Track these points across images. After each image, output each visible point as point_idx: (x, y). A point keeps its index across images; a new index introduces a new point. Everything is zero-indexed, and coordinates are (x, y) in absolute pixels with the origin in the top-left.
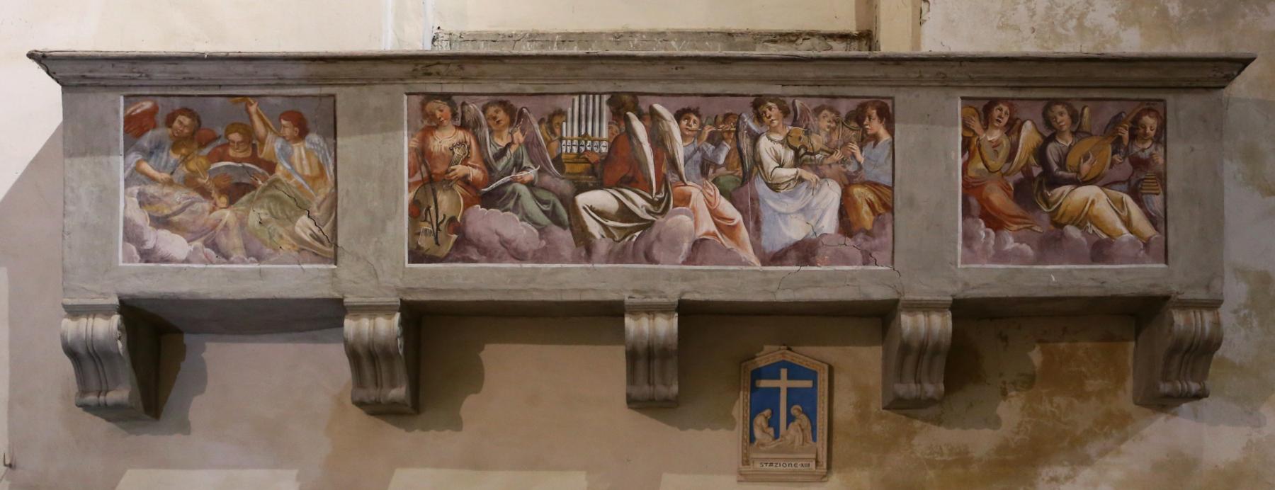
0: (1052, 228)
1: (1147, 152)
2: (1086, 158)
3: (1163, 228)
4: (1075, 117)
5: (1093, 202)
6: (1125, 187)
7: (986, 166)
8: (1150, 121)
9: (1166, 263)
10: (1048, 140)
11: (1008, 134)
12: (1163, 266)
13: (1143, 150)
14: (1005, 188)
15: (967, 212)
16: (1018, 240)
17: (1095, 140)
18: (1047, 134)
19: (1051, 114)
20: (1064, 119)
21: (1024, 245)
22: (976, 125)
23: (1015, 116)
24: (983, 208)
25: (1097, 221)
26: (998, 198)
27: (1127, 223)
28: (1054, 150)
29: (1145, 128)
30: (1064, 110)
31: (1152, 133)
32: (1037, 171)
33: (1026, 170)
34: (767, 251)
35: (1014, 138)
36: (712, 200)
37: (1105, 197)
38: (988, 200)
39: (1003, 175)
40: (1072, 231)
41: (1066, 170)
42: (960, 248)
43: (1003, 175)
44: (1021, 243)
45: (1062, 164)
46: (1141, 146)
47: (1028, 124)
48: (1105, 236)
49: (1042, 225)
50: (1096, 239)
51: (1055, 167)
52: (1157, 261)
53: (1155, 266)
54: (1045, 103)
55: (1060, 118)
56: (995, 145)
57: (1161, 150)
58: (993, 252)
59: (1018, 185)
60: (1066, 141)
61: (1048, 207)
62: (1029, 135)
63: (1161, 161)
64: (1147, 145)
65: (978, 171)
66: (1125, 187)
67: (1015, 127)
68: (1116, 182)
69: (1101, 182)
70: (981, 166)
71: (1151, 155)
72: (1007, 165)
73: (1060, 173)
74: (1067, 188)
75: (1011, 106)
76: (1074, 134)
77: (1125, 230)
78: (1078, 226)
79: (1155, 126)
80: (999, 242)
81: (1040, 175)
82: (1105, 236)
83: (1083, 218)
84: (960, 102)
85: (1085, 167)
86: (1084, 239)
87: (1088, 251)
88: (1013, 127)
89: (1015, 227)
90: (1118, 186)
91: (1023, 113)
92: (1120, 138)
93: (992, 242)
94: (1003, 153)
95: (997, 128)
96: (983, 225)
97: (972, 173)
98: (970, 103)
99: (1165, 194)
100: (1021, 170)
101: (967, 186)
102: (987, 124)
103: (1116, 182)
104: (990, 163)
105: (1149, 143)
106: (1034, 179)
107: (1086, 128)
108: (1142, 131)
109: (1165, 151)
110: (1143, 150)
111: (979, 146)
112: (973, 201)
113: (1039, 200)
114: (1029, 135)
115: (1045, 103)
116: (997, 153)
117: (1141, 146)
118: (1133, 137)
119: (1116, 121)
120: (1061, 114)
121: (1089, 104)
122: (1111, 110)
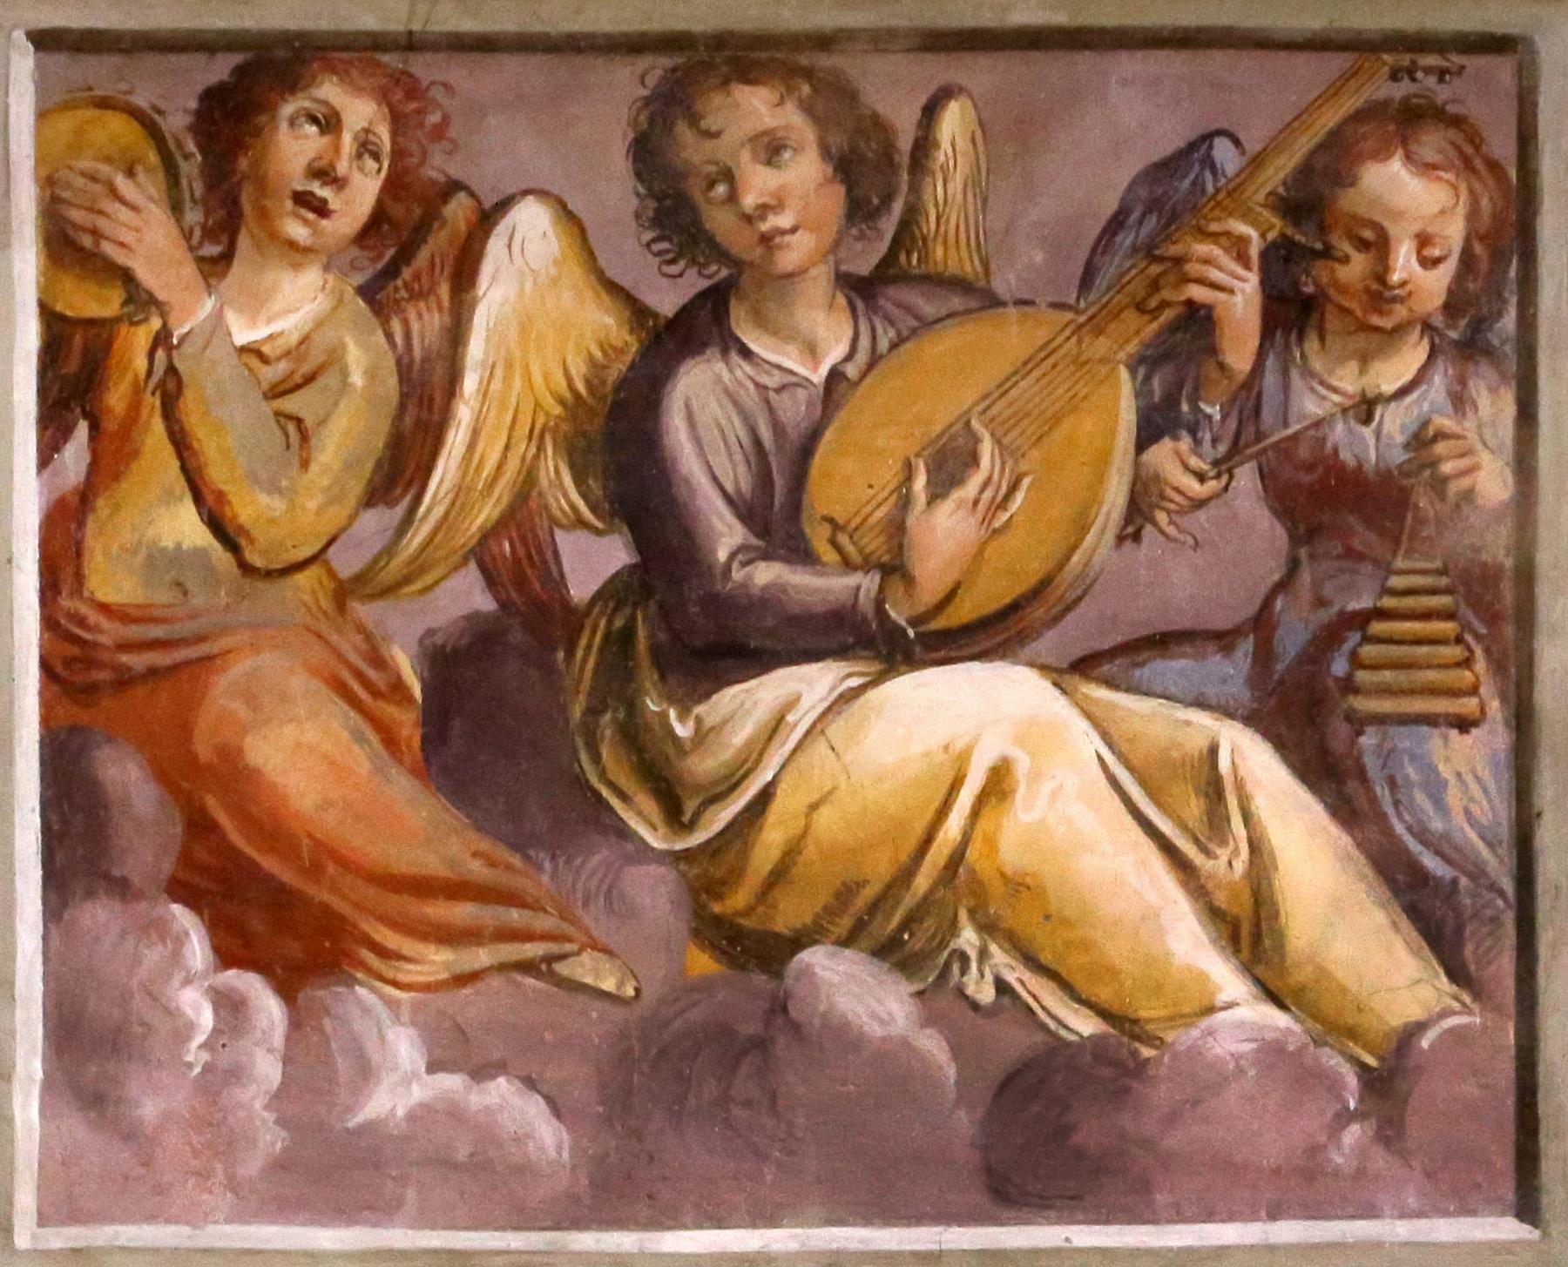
0: (702, 963)
1: (1395, 422)
2: (950, 463)
3: (1505, 965)
4: (871, 171)
5: (998, 784)
6: (1231, 671)
7: (217, 524)
8: (1413, 198)
9: (1528, 1208)
10: (673, 339)
11: (377, 295)
12: (1509, 1229)
13: (1366, 408)
14: (360, 686)
15: (78, 846)
16: (453, 1050)
17: (1012, 338)
18: (667, 300)
19: (690, 149)
20: (782, 183)
21: (501, 1095)
22: (149, 237)
23: (437, 165)
24: (199, 825)
25: (1022, 913)
26: (309, 754)
27: (1250, 930)
28: (712, 410)
29: (1380, 246)
30: (791, 119)
31: (1433, 285)
32: (592, 561)
33: (515, 557)
34: (248, 739)
35: (426, 323)
36: (456, 559)
37: (1089, 743)
38: (234, 775)
39: (344, 592)
40: (852, 990)
41: (801, 554)
42: (27, 1109)
43: (344, 592)
44: (481, 1073)
45: (776, 520)
46: (1348, 380)
47: (531, 224)
48: (1085, 1025)
49: (630, 949)
50: (1015, 1043)
51: (725, 535)
52: (1493, 1205)
53: (1446, 1230)
54: (657, 66)
55: (758, 183)
56: (292, 379)
57: (1494, 406)
58: (271, 1139)
59: (456, 664)
60: (808, 340)
61: (675, 816)
62: (534, 307)
63: (1493, 482)
64: (1394, 371)
65: (167, 564)
66: (1231, 671)
67: (437, 245)
68: (1162, 642)
69: (1046, 645)
70: (184, 527)
71: (1422, 440)
72: (376, 523)
73: (765, 574)
74: (812, 684)
75: (404, 101)
76: (861, 290)
77: (1227, 979)
78: (893, 953)
79: (1454, 232)
80: (317, 1069)
81: (615, 592)
82: (1085, 1025)
83: (917, 907)
84: (24, 63)
85: (944, 531)
86: (933, 1045)
87: (965, 1122)
88: (416, 246)
89: (438, 960)
90: (1173, 668)
91: (494, 136)
92: (1199, 323)
93: (268, 1070)
94: (349, 429)
95: (296, 253)
96: (198, 950)
97: (112, 579)
98: (99, 71)
99: (1523, 720)
100: (481, 554)
101: (73, 669)
102: (225, 221)
103: (1162, 642)
104: (251, 507)
105: (1409, 359)
106: (572, 620)
107: (950, 257)
108: (1356, 268)
109: (1527, 414)
110: (1366, 408)
111: (171, 389)
112: (125, 775)
113: (609, 769)
114: (534, 307)
115: (657, 66)
116: (299, 434)
117: (1348, 380)
118: (1291, 312)
119: (1172, 195)
120: (772, 149)
121: (979, 72)
122: (1125, 123)
